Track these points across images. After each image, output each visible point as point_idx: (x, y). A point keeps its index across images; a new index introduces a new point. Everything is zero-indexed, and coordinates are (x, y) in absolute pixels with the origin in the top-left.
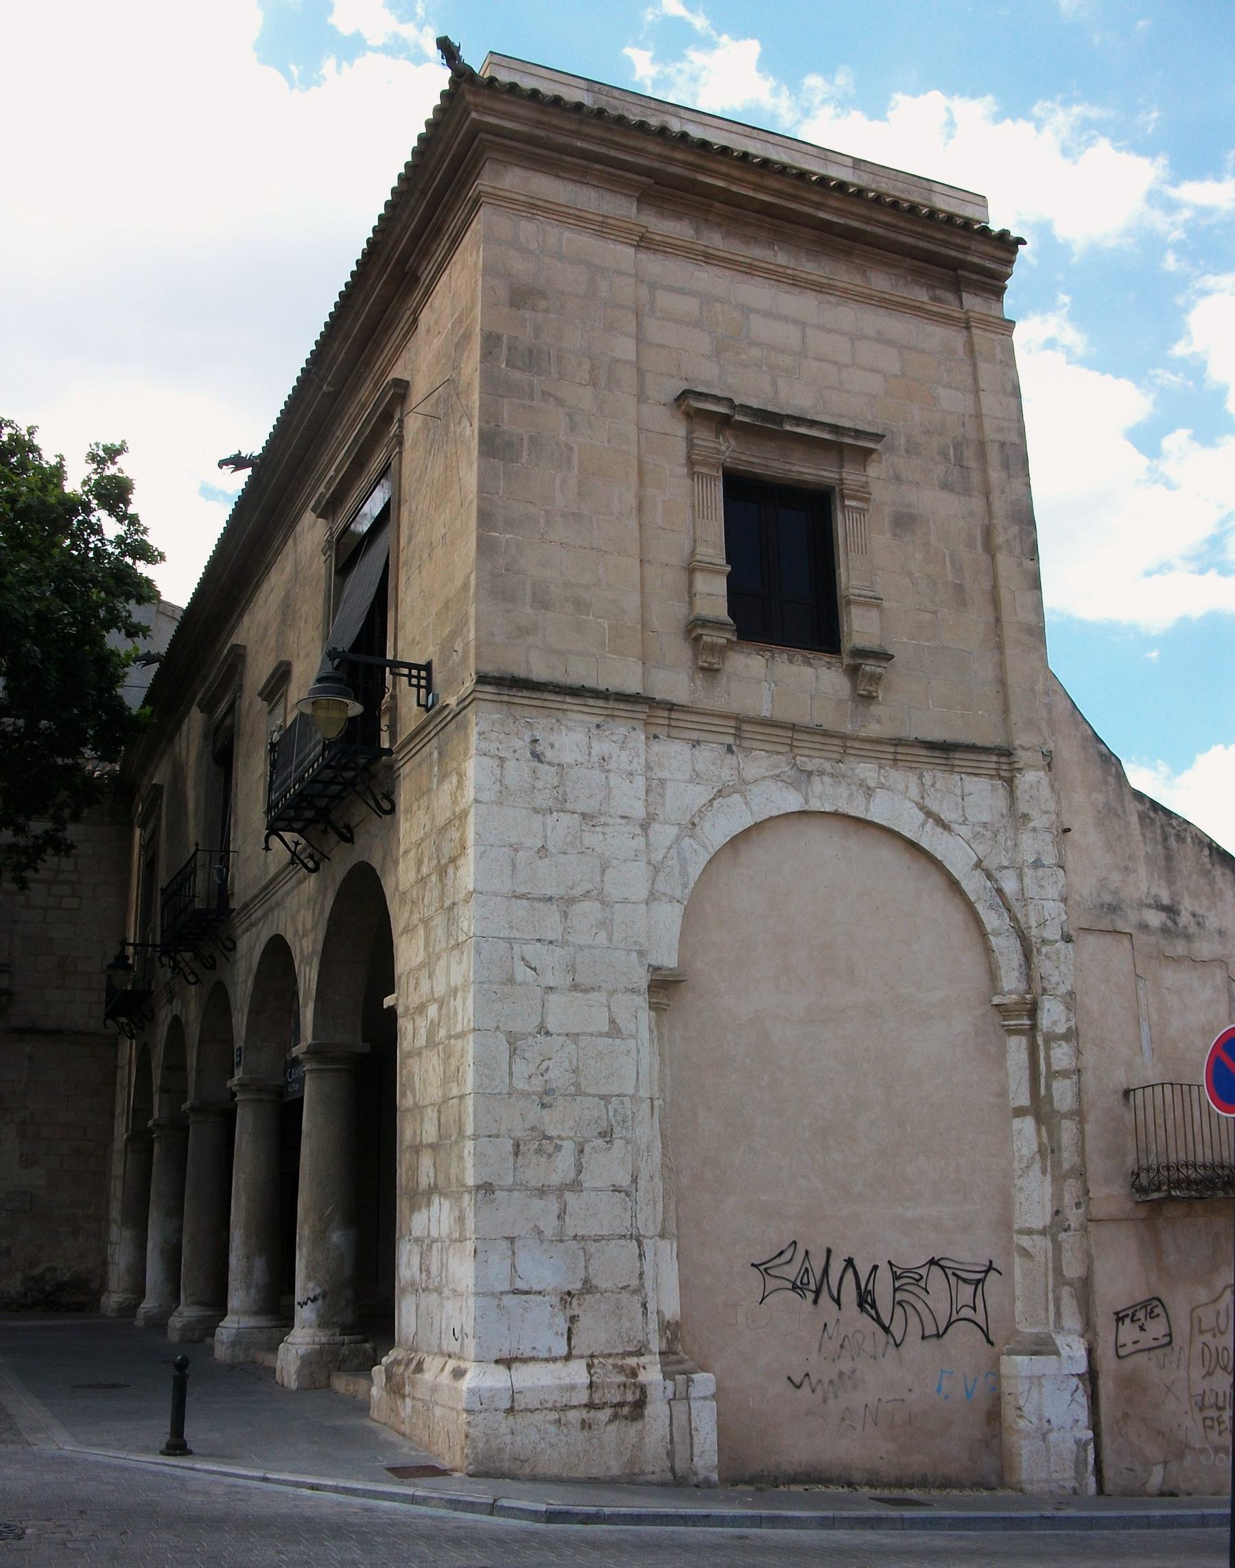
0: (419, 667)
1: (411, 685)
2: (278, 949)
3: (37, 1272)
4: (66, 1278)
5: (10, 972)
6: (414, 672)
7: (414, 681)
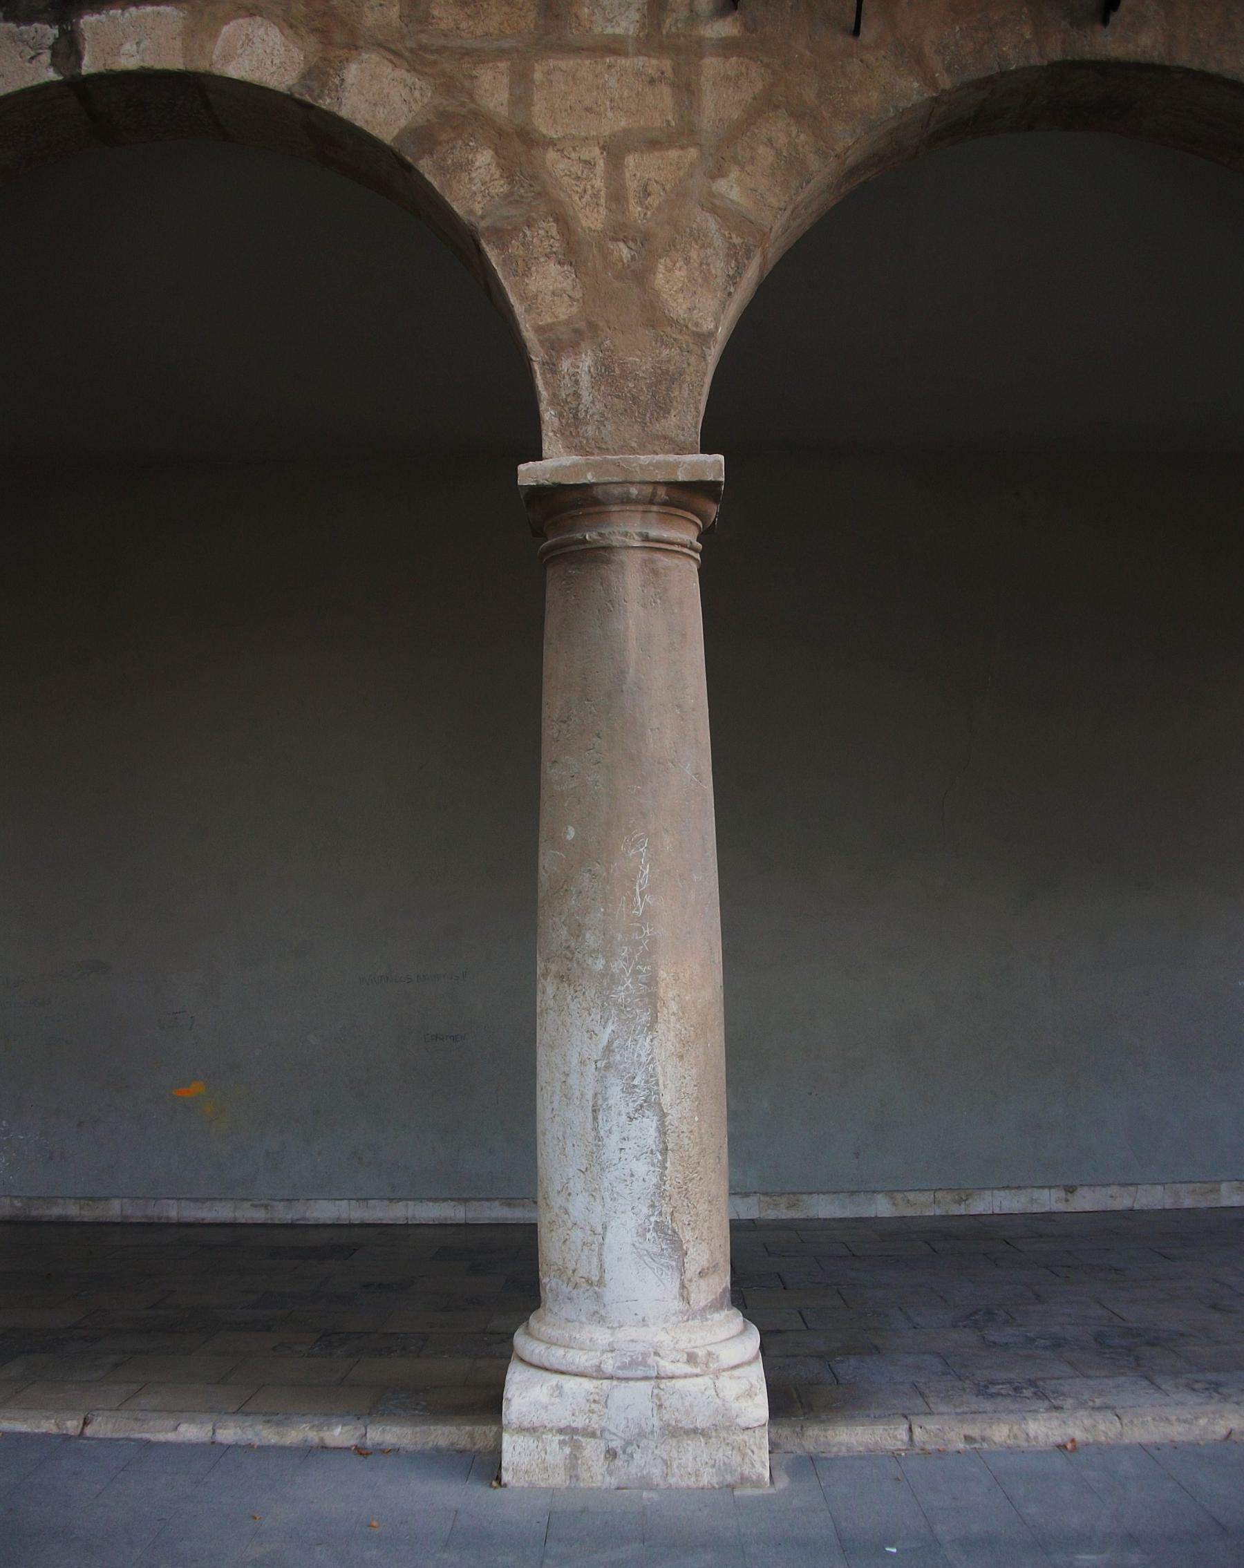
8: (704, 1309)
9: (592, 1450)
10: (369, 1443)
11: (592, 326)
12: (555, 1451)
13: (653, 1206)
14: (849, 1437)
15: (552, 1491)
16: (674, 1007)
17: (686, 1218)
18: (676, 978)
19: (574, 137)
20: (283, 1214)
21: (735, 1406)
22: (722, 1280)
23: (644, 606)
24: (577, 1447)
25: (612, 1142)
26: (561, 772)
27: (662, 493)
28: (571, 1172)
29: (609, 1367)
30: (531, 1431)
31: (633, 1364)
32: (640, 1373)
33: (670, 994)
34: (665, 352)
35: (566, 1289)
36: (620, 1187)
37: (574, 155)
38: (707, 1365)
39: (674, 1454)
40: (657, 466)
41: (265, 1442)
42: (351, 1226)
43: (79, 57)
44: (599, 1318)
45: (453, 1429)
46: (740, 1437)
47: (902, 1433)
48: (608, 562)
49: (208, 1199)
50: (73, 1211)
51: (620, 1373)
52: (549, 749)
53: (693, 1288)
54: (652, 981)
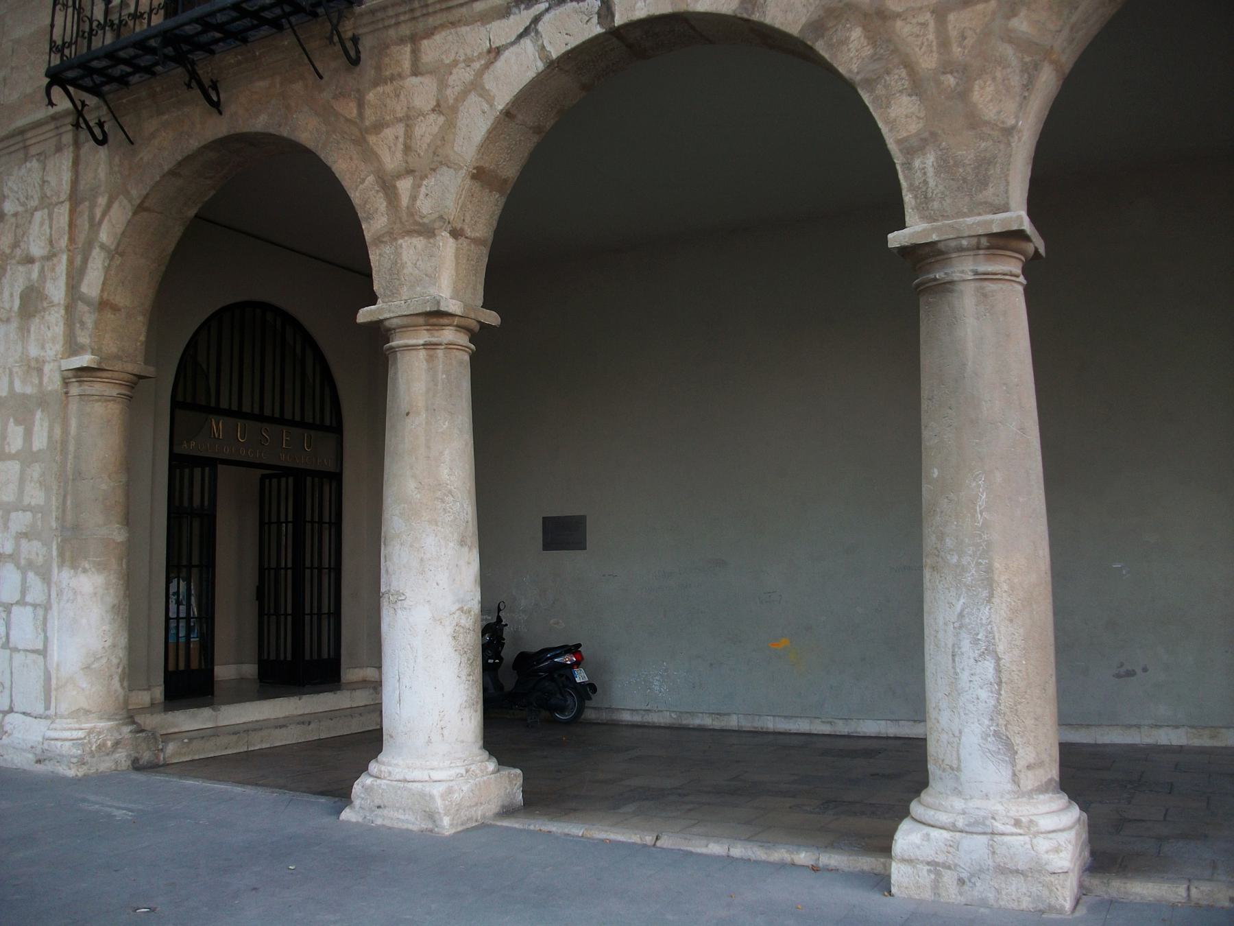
8: (1032, 791)
9: (949, 878)
10: (821, 864)
11: (933, 134)
12: (925, 876)
13: (992, 720)
14: (1143, 890)
15: (921, 902)
16: (1005, 587)
17: (1016, 729)
18: (1007, 567)
19: (913, 9)
20: (842, 728)
21: (1045, 856)
22: (1053, 772)
23: (978, 319)
24: (938, 874)
25: (965, 676)
26: (934, 432)
27: (984, 242)
28: (940, 695)
29: (960, 823)
30: (909, 861)
31: (976, 823)
32: (980, 829)
33: (1003, 578)
34: (983, 144)
35: (938, 772)
36: (970, 707)
37: (914, 21)
38: (1029, 828)
39: (1003, 886)
40: (979, 224)
41: (758, 858)
42: (888, 738)
43: (613, 16)
44: (958, 792)
45: (873, 860)
46: (1049, 878)
47: (1182, 891)
48: (952, 291)
49: (792, 717)
50: (708, 722)
51: (967, 829)
52: (924, 418)
53: (1022, 776)
54: (989, 570)
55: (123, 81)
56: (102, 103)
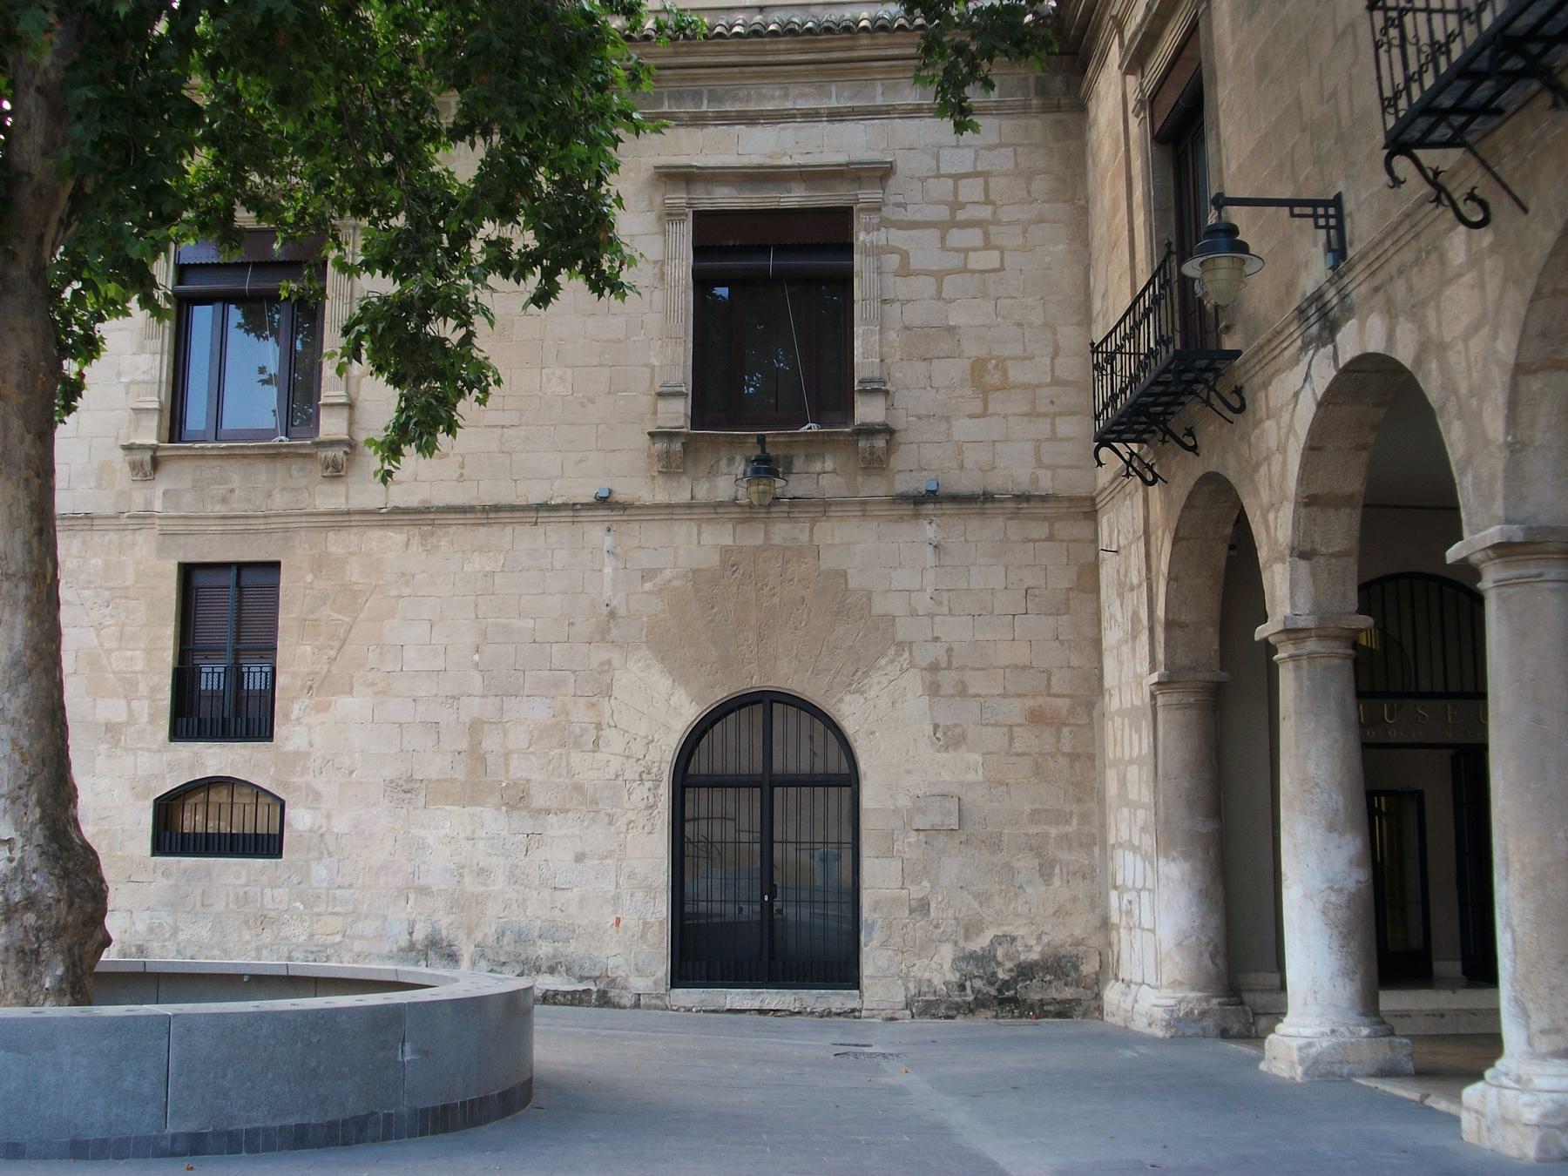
0: (1326, 204)
1: (1317, 227)
2: (1381, 398)
3: (979, 944)
4: (1034, 956)
5: (887, 392)
6: (1321, 211)
7: (1322, 222)
55: (1488, 110)
56: (1469, 155)
